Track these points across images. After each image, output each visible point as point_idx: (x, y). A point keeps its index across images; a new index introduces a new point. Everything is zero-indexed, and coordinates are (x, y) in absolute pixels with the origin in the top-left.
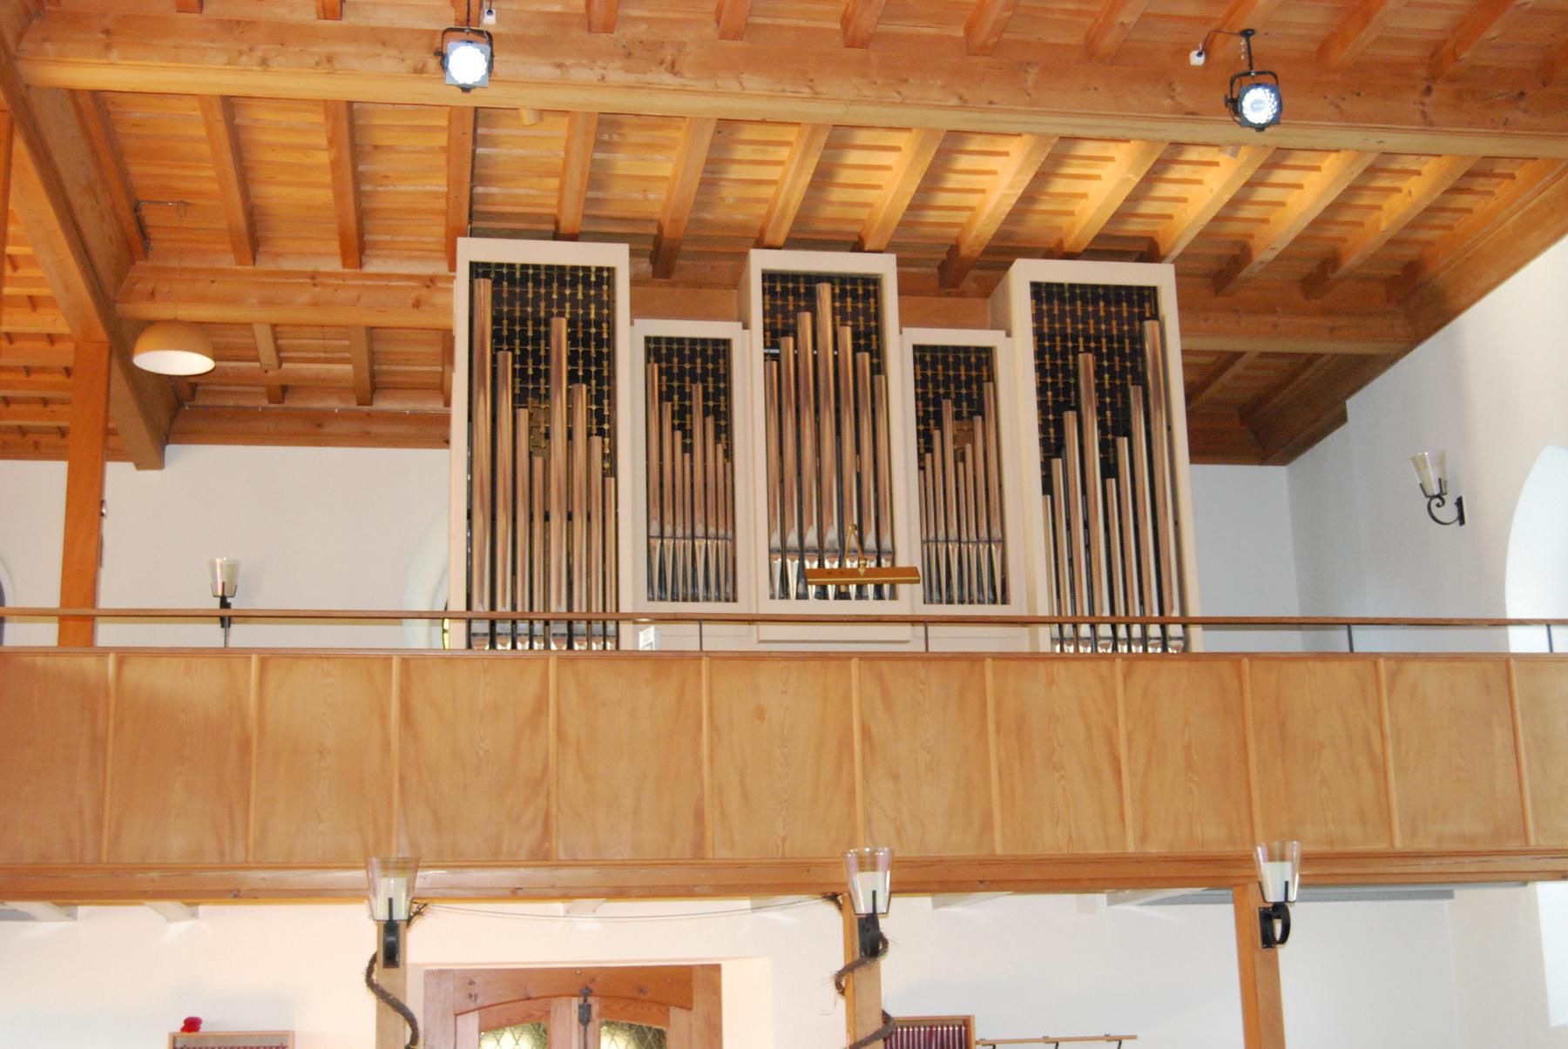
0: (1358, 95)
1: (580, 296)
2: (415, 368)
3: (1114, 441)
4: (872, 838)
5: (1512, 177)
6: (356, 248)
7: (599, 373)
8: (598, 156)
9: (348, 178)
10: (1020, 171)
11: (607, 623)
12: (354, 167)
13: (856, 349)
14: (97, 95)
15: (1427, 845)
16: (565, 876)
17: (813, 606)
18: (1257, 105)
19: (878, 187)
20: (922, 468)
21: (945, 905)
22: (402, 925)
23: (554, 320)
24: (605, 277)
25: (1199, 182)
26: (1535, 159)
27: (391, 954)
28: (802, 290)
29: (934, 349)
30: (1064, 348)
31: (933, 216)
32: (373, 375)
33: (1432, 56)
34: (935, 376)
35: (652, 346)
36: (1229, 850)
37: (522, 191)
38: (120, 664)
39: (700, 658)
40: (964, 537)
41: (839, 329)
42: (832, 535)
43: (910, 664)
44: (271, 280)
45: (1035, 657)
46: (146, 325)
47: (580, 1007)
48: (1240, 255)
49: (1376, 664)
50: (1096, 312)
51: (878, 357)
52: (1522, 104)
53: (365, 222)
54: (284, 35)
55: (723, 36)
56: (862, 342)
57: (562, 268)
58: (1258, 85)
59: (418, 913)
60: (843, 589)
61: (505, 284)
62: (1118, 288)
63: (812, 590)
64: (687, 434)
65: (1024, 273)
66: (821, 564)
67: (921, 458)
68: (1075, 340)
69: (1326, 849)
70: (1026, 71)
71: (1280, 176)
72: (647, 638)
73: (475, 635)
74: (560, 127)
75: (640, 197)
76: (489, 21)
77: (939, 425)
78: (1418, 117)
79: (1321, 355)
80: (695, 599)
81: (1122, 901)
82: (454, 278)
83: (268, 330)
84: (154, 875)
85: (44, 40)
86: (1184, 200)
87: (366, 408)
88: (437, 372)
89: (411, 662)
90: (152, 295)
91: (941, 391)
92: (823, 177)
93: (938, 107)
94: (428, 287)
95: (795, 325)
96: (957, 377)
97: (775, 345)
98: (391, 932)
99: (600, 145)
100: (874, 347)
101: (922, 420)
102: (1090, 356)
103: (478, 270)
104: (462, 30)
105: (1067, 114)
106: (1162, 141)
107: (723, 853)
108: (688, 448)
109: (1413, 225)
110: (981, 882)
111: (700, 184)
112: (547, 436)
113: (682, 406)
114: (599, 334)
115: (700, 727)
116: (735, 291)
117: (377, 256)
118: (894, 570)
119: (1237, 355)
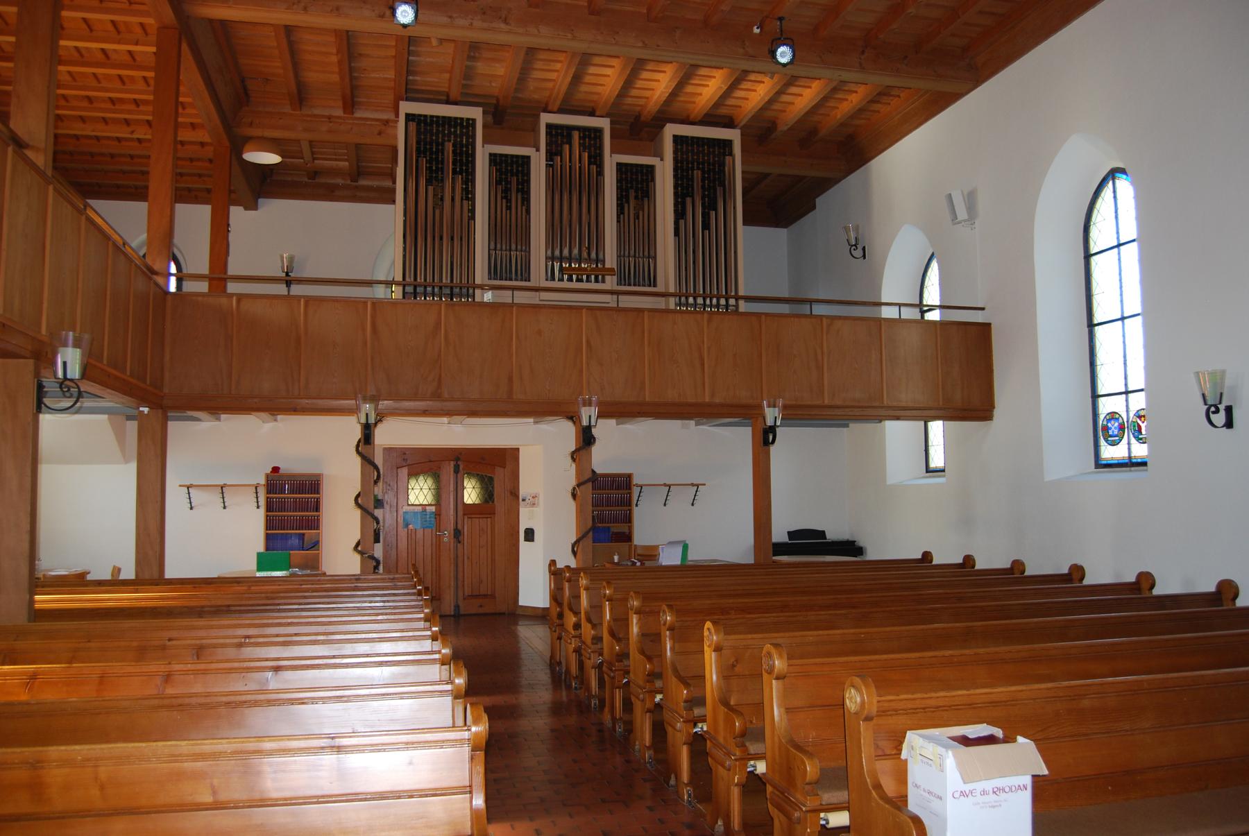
0: (831, 52)
5: (899, 96)
6: (350, 104)
7: (467, 171)
8: (469, 63)
10: (670, 81)
11: (469, 288)
15: (839, 403)
16: (449, 405)
18: (783, 55)
19: (604, 85)
20: (618, 221)
21: (622, 424)
23: (446, 143)
24: (471, 123)
25: (755, 91)
29: (626, 165)
32: (358, 167)
38: (239, 301)
39: (513, 307)
41: (583, 153)
42: (576, 251)
45: (667, 311)
47: (455, 465)
48: (772, 126)
49: (821, 320)
51: (600, 168)
57: (450, 118)
58: (783, 45)
59: (380, 420)
62: (714, 140)
63: (566, 277)
64: (509, 201)
65: (671, 130)
66: (570, 265)
68: (693, 163)
71: (793, 90)
72: (488, 297)
73: (407, 293)
74: (450, 48)
75: (488, 84)
77: (628, 202)
80: (511, 279)
81: (703, 424)
82: (398, 121)
84: (255, 400)
86: (747, 99)
89: (376, 303)
92: (577, 79)
97: (552, 160)
99: (470, 58)
100: (598, 163)
103: (409, 117)
108: (509, 208)
110: (639, 413)
112: (442, 199)
115: (512, 339)
118: (604, 269)
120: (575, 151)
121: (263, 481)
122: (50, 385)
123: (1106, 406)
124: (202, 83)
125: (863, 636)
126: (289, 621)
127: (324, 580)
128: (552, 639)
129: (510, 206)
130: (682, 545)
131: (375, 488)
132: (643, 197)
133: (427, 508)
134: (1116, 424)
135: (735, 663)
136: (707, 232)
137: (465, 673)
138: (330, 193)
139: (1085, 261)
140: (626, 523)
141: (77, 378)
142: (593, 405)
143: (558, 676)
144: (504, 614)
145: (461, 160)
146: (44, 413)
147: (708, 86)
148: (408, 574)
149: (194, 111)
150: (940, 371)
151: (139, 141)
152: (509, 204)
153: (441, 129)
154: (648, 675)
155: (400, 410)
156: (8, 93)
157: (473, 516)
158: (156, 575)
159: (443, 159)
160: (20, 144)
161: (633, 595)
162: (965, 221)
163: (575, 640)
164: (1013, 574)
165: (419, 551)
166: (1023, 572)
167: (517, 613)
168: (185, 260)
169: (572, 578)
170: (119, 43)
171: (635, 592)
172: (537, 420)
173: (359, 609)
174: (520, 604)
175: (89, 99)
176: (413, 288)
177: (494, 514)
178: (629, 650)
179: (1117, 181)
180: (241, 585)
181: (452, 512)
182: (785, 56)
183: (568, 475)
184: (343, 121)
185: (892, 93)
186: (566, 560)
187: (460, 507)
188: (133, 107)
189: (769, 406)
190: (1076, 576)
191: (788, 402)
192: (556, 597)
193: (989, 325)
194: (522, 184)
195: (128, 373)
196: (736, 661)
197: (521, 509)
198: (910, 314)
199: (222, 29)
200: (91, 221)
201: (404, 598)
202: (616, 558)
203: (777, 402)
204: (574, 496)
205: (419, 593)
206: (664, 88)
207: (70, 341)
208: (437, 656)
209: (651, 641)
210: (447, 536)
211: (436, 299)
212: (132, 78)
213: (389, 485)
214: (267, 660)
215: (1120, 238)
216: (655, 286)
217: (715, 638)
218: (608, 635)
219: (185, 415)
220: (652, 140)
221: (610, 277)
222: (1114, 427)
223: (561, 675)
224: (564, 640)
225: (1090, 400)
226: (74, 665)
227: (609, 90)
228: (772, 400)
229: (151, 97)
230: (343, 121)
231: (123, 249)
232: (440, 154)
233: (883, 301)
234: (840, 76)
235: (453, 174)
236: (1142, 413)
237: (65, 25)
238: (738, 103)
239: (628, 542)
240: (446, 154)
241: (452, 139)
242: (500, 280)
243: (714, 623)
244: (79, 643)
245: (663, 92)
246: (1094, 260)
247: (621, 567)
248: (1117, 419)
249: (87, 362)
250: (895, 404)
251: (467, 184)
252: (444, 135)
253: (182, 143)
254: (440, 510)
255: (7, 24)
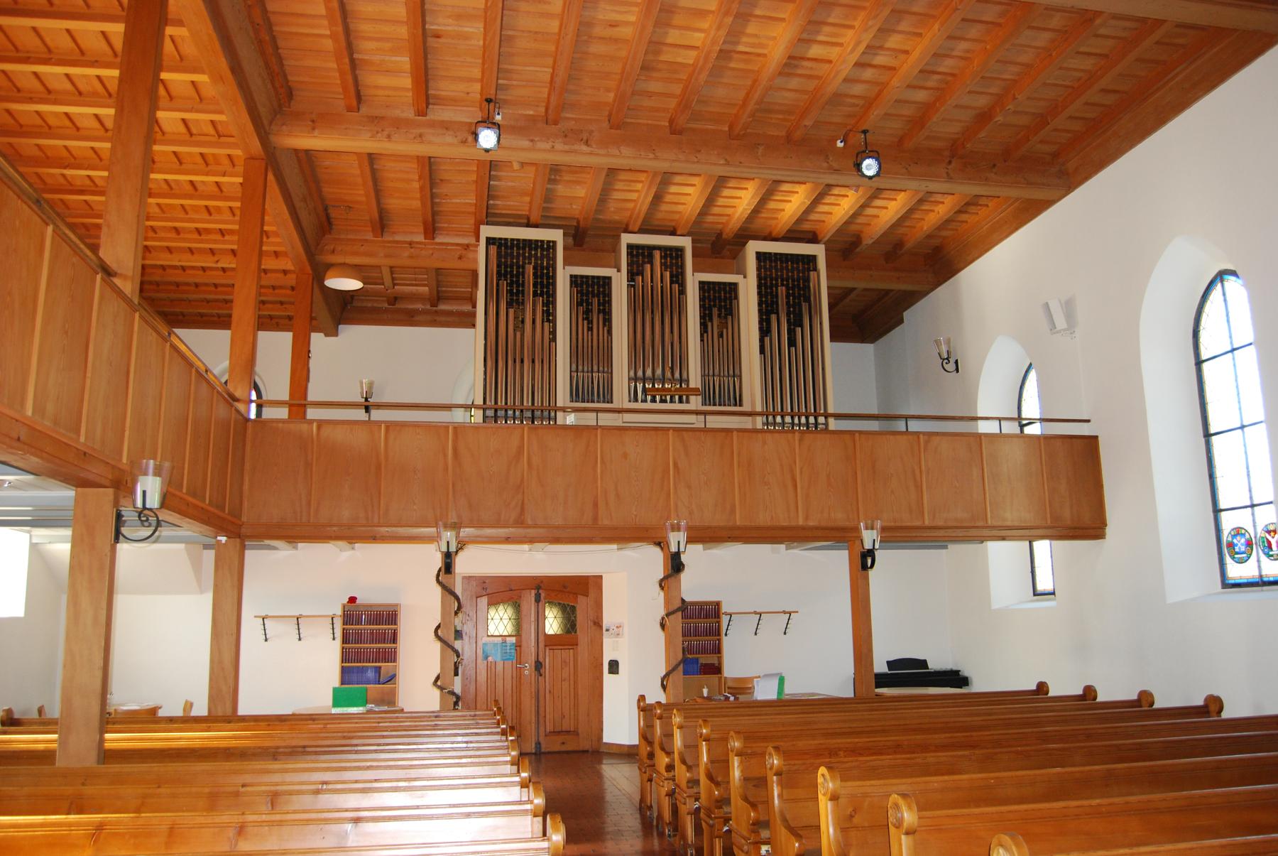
0: (917, 163)
1: (539, 255)
2: (458, 289)
3: (794, 329)
4: (678, 515)
5: (987, 206)
6: (431, 230)
7: (548, 292)
8: (549, 186)
9: (429, 195)
10: (752, 197)
11: (551, 410)
12: (431, 189)
13: (672, 282)
14: (307, 152)
15: (940, 523)
16: (531, 532)
17: (649, 405)
18: (869, 167)
19: (684, 204)
20: (702, 340)
21: (709, 549)
22: (453, 554)
23: (527, 266)
24: (551, 245)
25: (839, 205)
26: (999, 197)
27: (448, 567)
28: (646, 254)
29: (709, 283)
30: (771, 283)
31: (710, 219)
32: (438, 292)
33: (952, 146)
34: (709, 296)
35: (573, 279)
36: (847, 524)
37: (512, 203)
38: (319, 428)
39: (597, 429)
40: (722, 374)
41: (664, 273)
42: (659, 372)
43: (698, 433)
44: (389, 245)
45: (755, 431)
46: (329, 266)
47: (535, 594)
48: (856, 240)
49: (918, 437)
50: (787, 266)
51: (682, 286)
52: (994, 170)
53: (436, 217)
54: (398, 124)
55: (611, 128)
56: (674, 279)
57: (530, 241)
58: (869, 157)
59: (461, 548)
60: (663, 398)
61: (503, 248)
62: (798, 255)
63: (649, 398)
64: (590, 322)
65: (753, 247)
66: (653, 385)
67: (702, 336)
68: (777, 280)
69: (892, 524)
70: (758, 148)
71: (878, 203)
72: (571, 419)
73: (487, 417)
74: (531, 172)
75: (569, 207)
76: (498, 118)
77: (711, 320)
78: (945, 175)
79: (892, 290)
80: (593, 401)
81: (793, 548)
82: (479, 245)
83: (388, 270)
84: (335, 528)
85: (283, 125)
86: (831, 213)
87: (435, 308)
88: (468, 291)
89: (458, 429)
90: (333, 252)
91: (712, 303)
92: (658, 198)
93: (715, 164)
94: (466, 249)
95: (643, 270)
96: (720, 297)
97: (633, 280)
98: (448, 559)
99: (550, 181)
100: (680, 282)
101: (703, 317)
102: (784, 288)
103: (490, 241)
104: (486, 122)
105: (777, 169)
106: (822, 183)
107: (606, 522)
108: (590, 329)
109: (939, 228)
110: (729, 537)
111: (598, 201)
112: (523, 322)
113: (587, 309)
114: (548, 273)
115: (597, 462)
116: (613, 254)
117: (441, 234)
118: (688, 389)
119: (853, 289)
120: (656, 270)
121: (339, 612)
122: (129, 514)
123: (1229, 521)
124: (286, 212)
125: (992, 781)
126: (368, 764)
127: (402, 717)
128: (642, 781)
129: (592, 328)
130: (778, 678)
131: (456, 619)
132: (726, 315)
133: (508, 639)
134: (1243, 540)
135: (853, 813)
136: (793, 349)
137: (562, 828)
138: (409, 318)
139: (1196, 368)
140: (715, 653)
141: (156, 507)
142: (682, 529)
143: (649, 824)
144: (587, 751)
145: (542, 282)
146: (122, 542)
147: (790, 201)
148: (487, 710)
149: (278, 240)
150: (1046, 488)
151: (224, 270)
152: (590, 326)
153: (521, 252)
154: (753, 824)
155: (482, 537)
156: (98, 227)
157: (555, 647)
158: (229, 712)
159: (523, 281)
160: (108, 272)
161: (734, 735)
162: (1064, 330)
163: (669, 783)
164: (1141, 707)
165: (500, 684)
166: (1152, 704)
167: (601, 750)
168: (264, 386)
169: (664, 715)
170: (207, 174)
171: (736, 732)
172: (620, 546)
173: (441, 750)
174: (604, 741)
175: (177, 230)
176: (495, 412)
177: (577, 645)
178: (730, 794)
179: (1225, 283)
180: (316, 722)
181: (533, 643)
182: (870, 169)
183: (656, 604)
184: (423, 246)
185: (980, 203)
186: (656, 695)
187: (541, 638)
188: (219, 237)
189: (867, 528)
190: (1213, 708)
191: (886, 524)
192: (645, 736)
193: (1096, 437)
194: (604, 306)
195: (207, 502)
196: (854, 810)
197: (605, 640)
198: (1010, 428)
199: (307, 159)
200: (174, 347)
201: (489, 739)
202: (705, 692)
203: (875, 523)
204: (663, 626)
205: (504, 733)
206: (747, 205)
207: (151, 470)
208: (528, 807)
209: (754, 786)
210: (528, 669)
211: (517, 422)
212: (218, 209)
213: (469, 615)
214: (347, 810)
215: (1234, 342)
216: (741, 405)
217: (830, 785)
218: (706, 779)
219: (262, 543)
220: (734, 258)
221: (694, 397)
222: (1240, 543)
223: (653, 820)
224: (656, 782)
225: (1212, 515)
226: (143, 815)
227: (690, 209)
228: (869, 522)
229: (236, 227)
230: (423, 246)
231: (206, 376)
232: (521, 277)
233: (979, 416)
234: (927, 187)
235: (533, 297)
236: (1271, 528)
237: (156, 159)
238: (823, 217)
239: (718, 674)
240: (526, 276)
241: (533, 261)
242: (592, 402)
243: (830, 768)
244: (149, 788)
245: (745, 209)
246: (1205, 366)
247: (714, 702)
248: (1244, 535)
249: (167, 491)
250: (999, 523)
251: (548, 306)
252: (524, 258)
253: (265, 271)
254: (521, 642)
255: (101, 159)
